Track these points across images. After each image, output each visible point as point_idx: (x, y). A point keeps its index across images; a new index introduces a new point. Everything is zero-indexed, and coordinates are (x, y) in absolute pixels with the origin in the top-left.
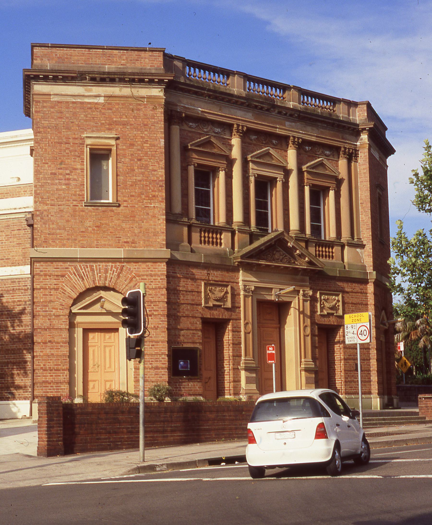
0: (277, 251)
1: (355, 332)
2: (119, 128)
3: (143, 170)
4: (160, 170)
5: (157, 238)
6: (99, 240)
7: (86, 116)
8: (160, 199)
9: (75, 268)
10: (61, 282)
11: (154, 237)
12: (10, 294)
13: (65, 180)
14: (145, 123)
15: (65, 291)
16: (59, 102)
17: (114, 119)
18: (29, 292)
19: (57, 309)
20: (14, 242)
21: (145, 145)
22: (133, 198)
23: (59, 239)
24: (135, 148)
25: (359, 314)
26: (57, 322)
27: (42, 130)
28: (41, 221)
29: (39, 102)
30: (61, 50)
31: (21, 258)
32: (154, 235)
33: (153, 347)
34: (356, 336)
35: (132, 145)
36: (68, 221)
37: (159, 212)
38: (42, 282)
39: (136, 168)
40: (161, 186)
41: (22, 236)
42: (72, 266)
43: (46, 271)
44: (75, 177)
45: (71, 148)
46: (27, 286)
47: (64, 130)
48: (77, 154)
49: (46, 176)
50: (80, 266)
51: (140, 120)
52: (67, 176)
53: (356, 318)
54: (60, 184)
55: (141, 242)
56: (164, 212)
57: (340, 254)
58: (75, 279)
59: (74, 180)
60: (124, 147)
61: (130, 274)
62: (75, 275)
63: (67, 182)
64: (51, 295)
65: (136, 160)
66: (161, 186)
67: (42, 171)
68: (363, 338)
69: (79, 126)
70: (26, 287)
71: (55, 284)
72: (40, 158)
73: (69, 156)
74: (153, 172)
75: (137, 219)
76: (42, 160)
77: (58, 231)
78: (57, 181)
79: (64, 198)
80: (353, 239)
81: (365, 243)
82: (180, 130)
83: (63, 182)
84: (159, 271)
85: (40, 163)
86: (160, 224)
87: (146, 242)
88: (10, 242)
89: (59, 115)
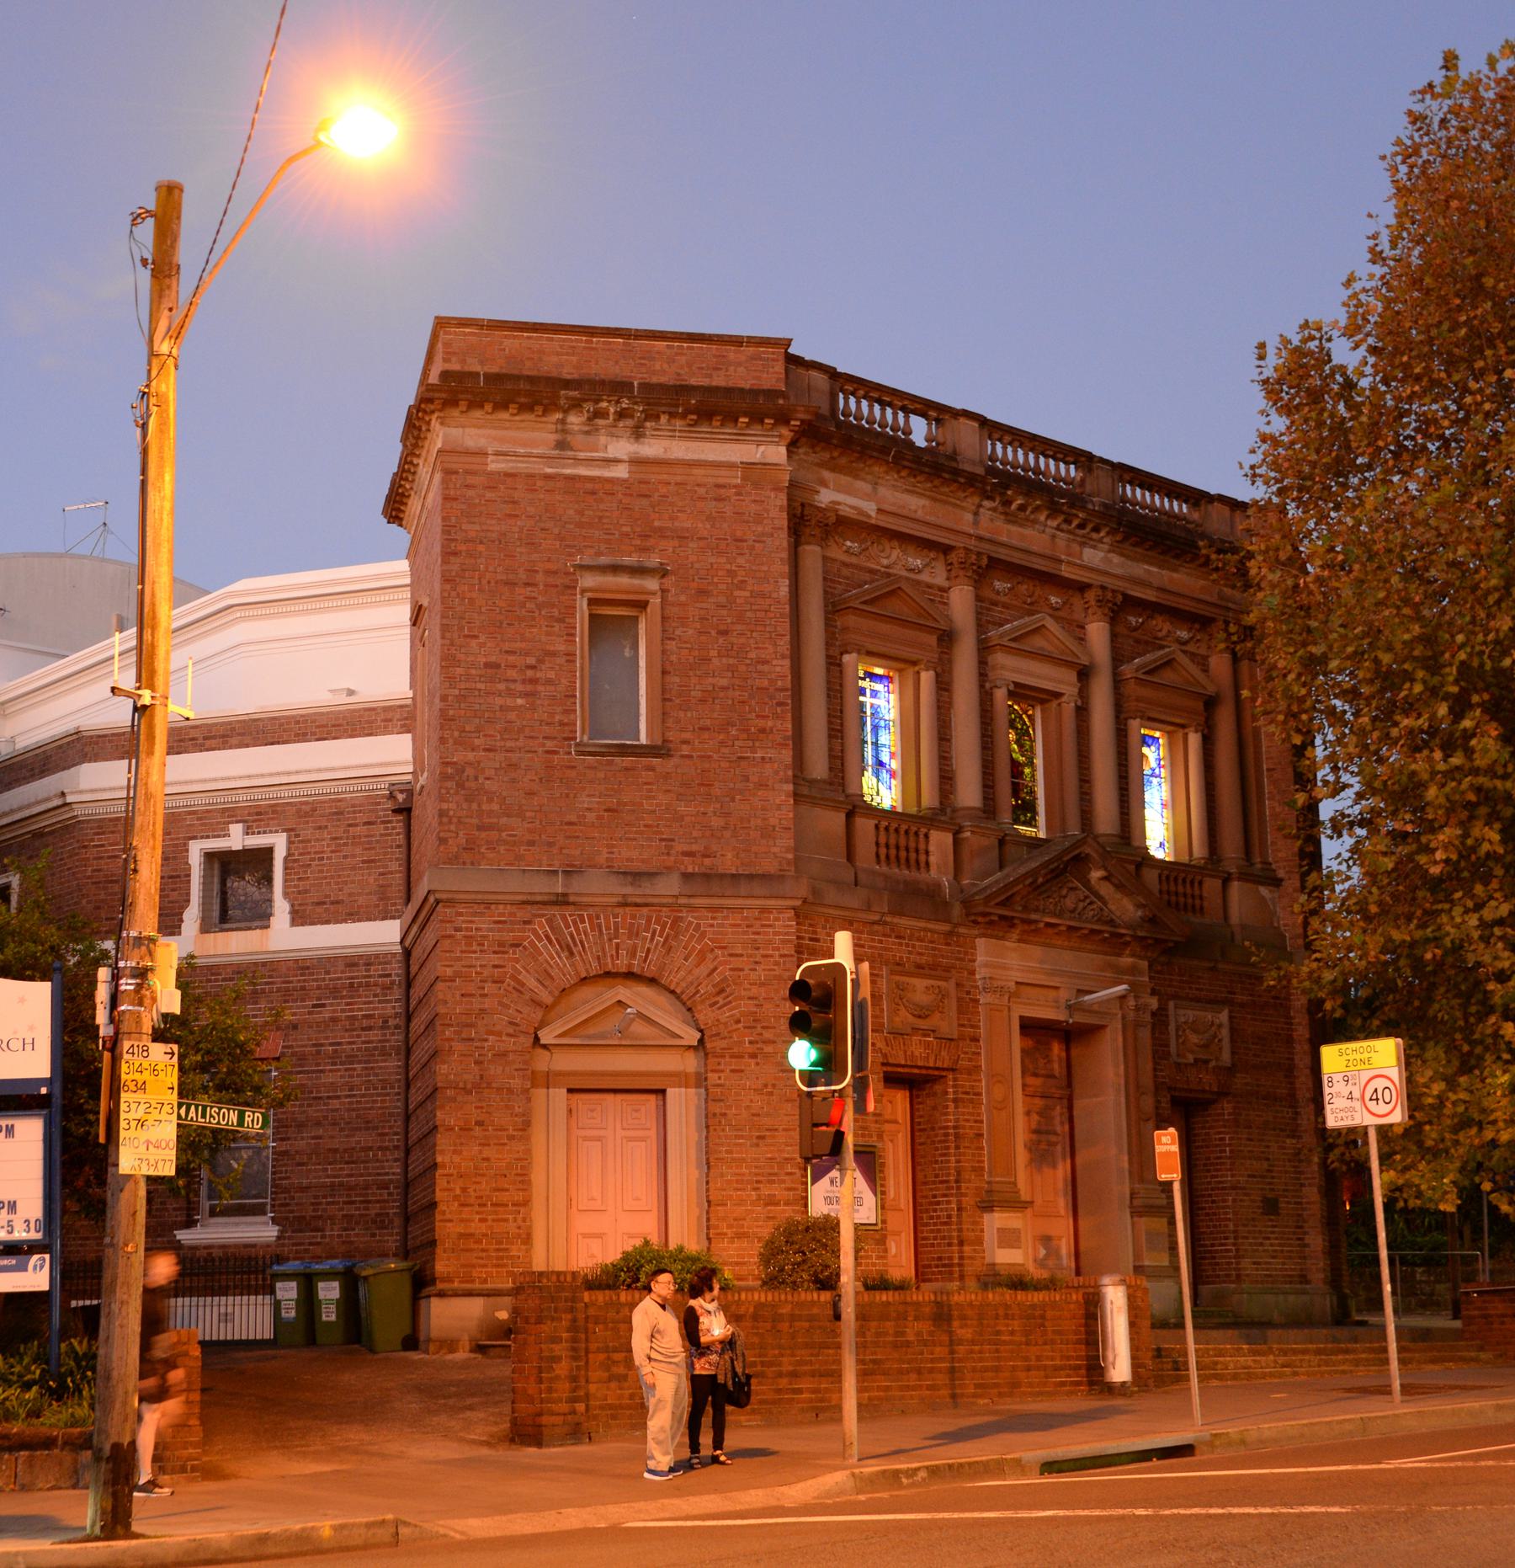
0: (1071, 889)
1: (1357, 1094)
2: (669, 545)
3: (731, 661)
4: (780, 662)
5: (771, 843)
6: (613, 846)
7: (581, 513)
8: (779, 740)
9: (550, 922)
10: (510, 960)
11: (764, 842)
12: (342, 997)
13: (524, 682)
14: (739, 534)
15: (523, 985)
16: (507, 475)
17: (656, 524)
18: (397, 993)
19: (499, 1034)
20: (354, 856)
21: (736, 593)
22: (706, 735)
23: (506, 842)
24: (711, 600)
25: (1365, 1044)
26: (499, 1071)
27: (463, 548)
28: (457, 793)
29: (456, 473)
30: (515, 337)
31: (374, 898)
32: (762, 836)
33: (761, 1142)
34: (1357, 1105)
35: (703, 593)
36: (531, 794)
37: (777, 773)
38: (459, 959)
39: (713, 653)
40: (780, 704)
41: (378, 842)
42: (542, 916)
43: (471, 929)
44: (552, 675)
45: (541, 599)
46: (389, 975)
47: (523, 550)
48: (556, 612)
49: (473, 672)
50: (564, 918)
51: (725, 525)
52: (530, 673)
53: (1358, 1056)
54: (511, 693)
55: (729, 856)
56: (790, 773)
57: (1220, 901)
58: (549, 953)
59: (549, 682)
60: (683, 598)
61: (699, 941)
62: (550, 941)
63: (529, 688)
64: (485, 995)
65: (713, 633)
66: (780, 704)
67: (462, 657)
68: (1382, 1108)
69: (562, 539)
70: (387, 980)
71: (496, 966)
72: (456, 622)
73: (534, 619)
74: (760, 667)
75: (716, 790)
76: (461, 629)
77: (504, 820)
78: (502, 686)
79: (521, 730)
80: (1252, 865)
81: (1281, 874)
82: (825, 558)
83: (519, 687)
84: (775, 934)
85: (455, 636)
86: (779, 807)
87: (742, 855)
88: (345, 857)
89: (508, 509)
